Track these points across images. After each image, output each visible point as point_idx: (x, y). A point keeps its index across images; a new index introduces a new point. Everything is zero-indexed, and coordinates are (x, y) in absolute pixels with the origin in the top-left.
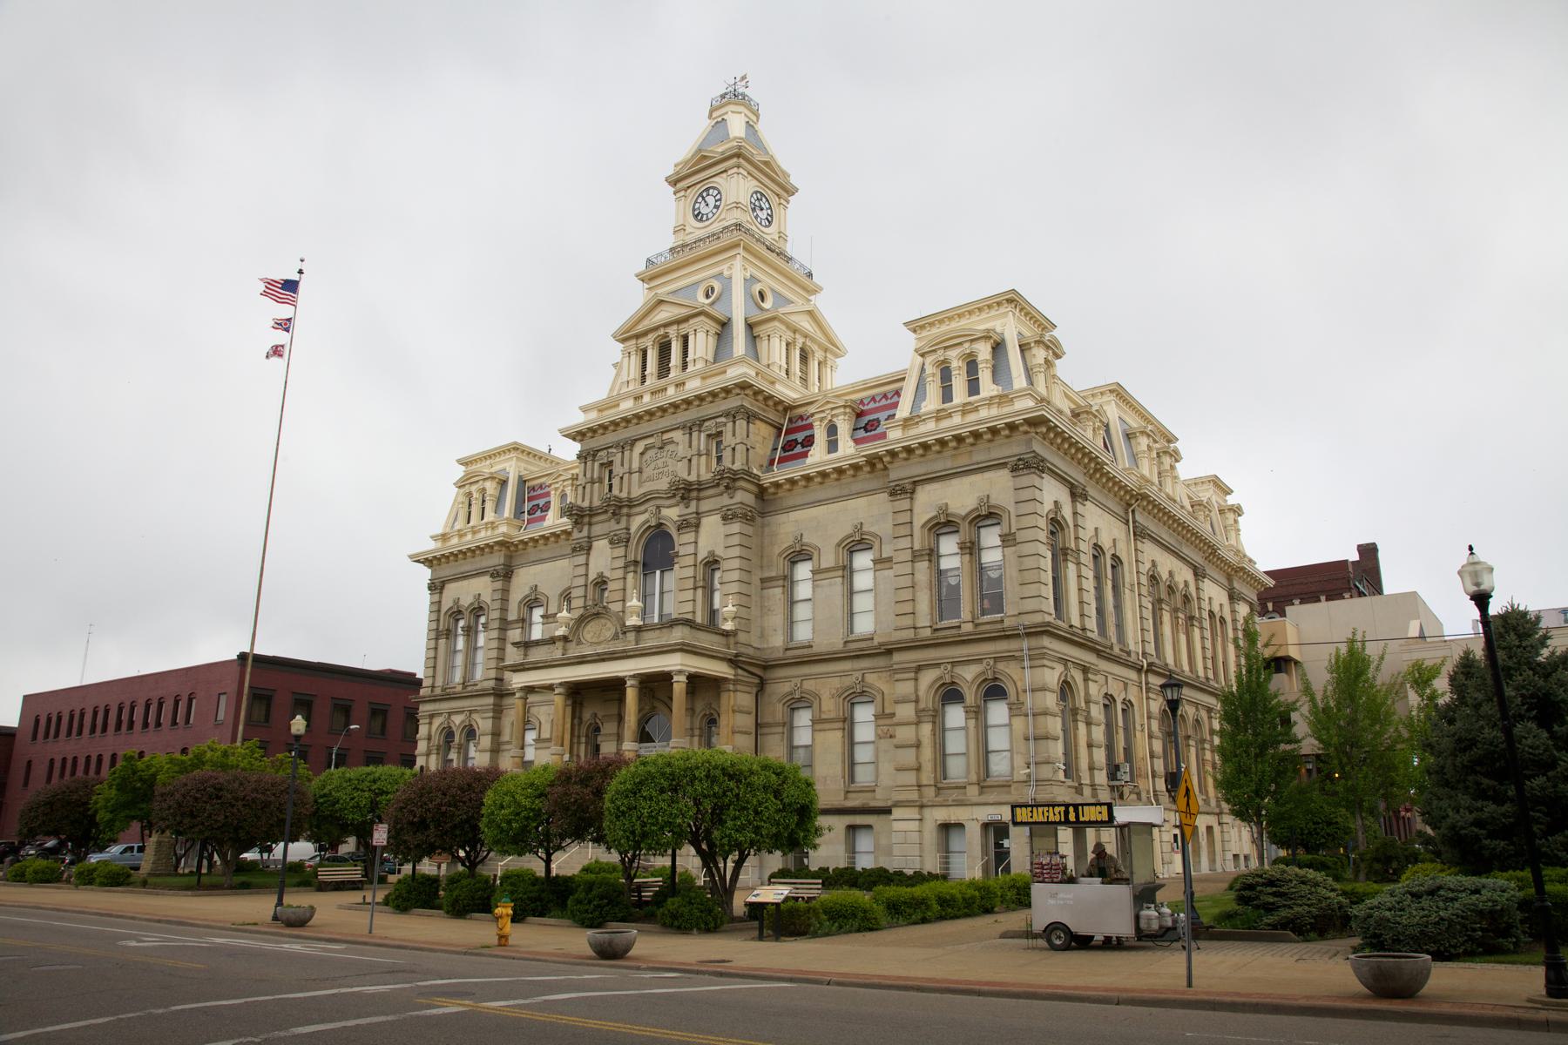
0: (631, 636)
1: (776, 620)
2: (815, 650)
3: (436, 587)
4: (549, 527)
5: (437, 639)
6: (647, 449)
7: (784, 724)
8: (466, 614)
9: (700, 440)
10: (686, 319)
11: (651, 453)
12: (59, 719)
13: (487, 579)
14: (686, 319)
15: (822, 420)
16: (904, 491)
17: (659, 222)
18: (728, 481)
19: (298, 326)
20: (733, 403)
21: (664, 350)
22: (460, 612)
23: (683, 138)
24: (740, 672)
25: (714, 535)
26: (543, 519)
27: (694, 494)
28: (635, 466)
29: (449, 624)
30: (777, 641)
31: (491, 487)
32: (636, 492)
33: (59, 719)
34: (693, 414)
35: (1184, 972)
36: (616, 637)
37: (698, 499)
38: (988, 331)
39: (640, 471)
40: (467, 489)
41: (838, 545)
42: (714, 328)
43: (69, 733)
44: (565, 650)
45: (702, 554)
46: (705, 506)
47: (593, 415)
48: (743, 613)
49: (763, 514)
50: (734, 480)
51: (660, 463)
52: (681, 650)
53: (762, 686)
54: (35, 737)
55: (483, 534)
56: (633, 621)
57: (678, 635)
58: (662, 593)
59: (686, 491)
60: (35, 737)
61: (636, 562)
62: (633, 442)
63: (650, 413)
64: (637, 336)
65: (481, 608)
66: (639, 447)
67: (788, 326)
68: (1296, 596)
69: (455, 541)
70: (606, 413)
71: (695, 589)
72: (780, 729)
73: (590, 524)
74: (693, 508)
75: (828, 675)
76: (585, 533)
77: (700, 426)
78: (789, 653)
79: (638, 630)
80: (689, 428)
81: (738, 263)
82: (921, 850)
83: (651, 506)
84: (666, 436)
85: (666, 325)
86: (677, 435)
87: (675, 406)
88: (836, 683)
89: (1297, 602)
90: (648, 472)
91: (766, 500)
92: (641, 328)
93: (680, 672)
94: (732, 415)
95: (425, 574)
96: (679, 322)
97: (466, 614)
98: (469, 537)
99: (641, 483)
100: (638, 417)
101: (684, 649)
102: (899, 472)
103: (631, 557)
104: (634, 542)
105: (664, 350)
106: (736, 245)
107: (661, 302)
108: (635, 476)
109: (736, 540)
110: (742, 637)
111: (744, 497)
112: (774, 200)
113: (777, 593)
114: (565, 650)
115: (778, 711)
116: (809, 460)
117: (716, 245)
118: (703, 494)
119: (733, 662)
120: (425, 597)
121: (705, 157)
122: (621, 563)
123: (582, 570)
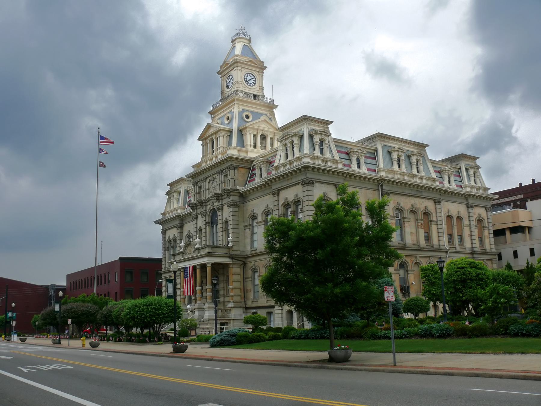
0: (197, 251)
1: (248, 241)
2: (258, 251)
3: (164, 232)
4: (257, 183)
5: (165, 251)
7: (251, 277)
8: (292, 205)
11: (211, 182)
12: (82, 281)
13: (176, 229)
15: (258, 166)
16: (276, 193)
18: (228, 193)
19: (96, 150)
20: (229, 164)
22: (288, 205)
24: (234, 260)
25: (227, 213)
26: (254, 180)
28: (207, 187)
29: (170, 245)
30: (249, 248)
31: (296, 140)
33: (82, 281)
35: (392, 361)
36: (194, 252)
37: (222, 199)
38: (295, 132)
39: (209, 189)
40: (284, 142)
41: (262, 213)
42: (226, 134)
43: (105, 283)
44: (183, 256)
45: (224, 219)
46: (225, 201)
48: (235, 239)
49: (244, 202)
50: (229, 193)
52: (208, 256)
53: (244, 265)
54: (71, 290)
55: (295, 164)
56: (198, 246)
57: (207, 251)
58: (217, 233)
59: (218, 197)
60: (71, 290)
61: (208, 222)
65: (299, 201)
66: (208, 180)
67: (253, 129)
68: (528, 198)
69: (282, 169)
71: (223, 231)
72: (250, 279)
73: (197, 209)
74: (220, 203)
75: (259, 260)
76: (195, 213)
77: (222, 172)
78: (252, 252)
79: (199, 249)
81: (236, 106)
82: (282, 320)
83: (210, 203)
85: (212, 135)
86: (216, 176)
88: (263, 263)
89: (529, 200)
90: (211, 189)
91: (243, 197)
93: (208, 263)
94: (229, 168)
95: (160, 227)
97: (292, 205)
98: (288, 166)
101: (209, 255)
102: (275, 186)
103: (207, 221)
104: (208, 215)
105: (263, 137)
106: (234, 100)
108: (207, 191)
109: (231, 214)
110: (235, 248)
111: (234, 198)
112: (256, 74)
113: (248, 230)
114: (183, 256)
115: (249, 273)
116: (255, 182)
119: (231, 257)
120: (161, 236)
122: (204, 223)
123: (195, 226)
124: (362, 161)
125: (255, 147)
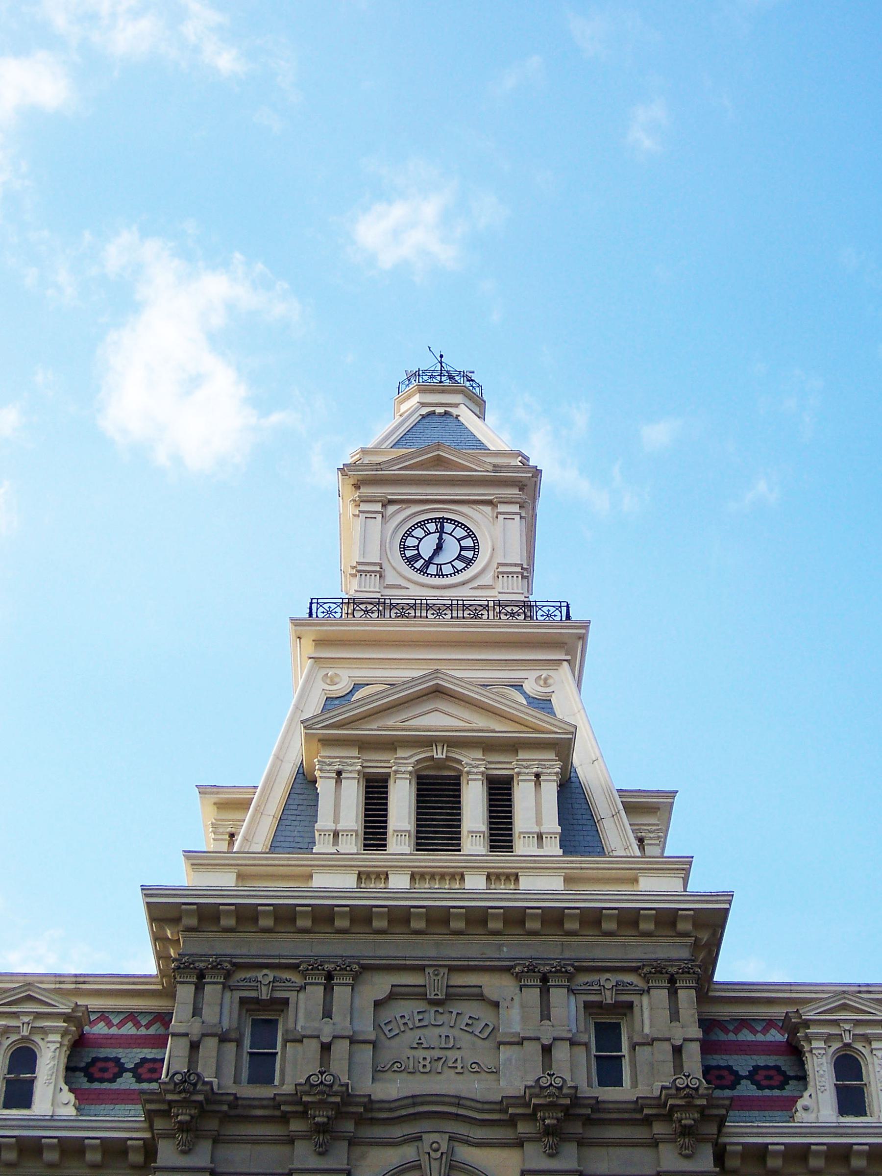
6: (393, 996)
9: (566, 1010)
10: (512, 746)
11: (406, 1008)
14: (512, 746)
17: (327, 547)
21: (438, 797)
23: (381, 423)
27: (212, 1125)
32: (391, 1089)
34: (549, 949)
47: (226, 880)
51: (431, 1036)
62: (365, 969)
63: (400, 918)
64: (364, 745)
66: (380, 985)
70: (425, 886)
80: (542, 977)
84: (459, 980)
87: (477, 919)
92: (392, 725)
96: (489, 746)
99: (377, 1072)
100: (362, 917)
105: (438, 797)
107: (438, 692)
117: (474, 628)
118: (595, 1133)
121: (439, 462)
124: (50, 1060)
125: (375, 832)
